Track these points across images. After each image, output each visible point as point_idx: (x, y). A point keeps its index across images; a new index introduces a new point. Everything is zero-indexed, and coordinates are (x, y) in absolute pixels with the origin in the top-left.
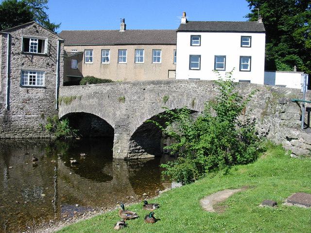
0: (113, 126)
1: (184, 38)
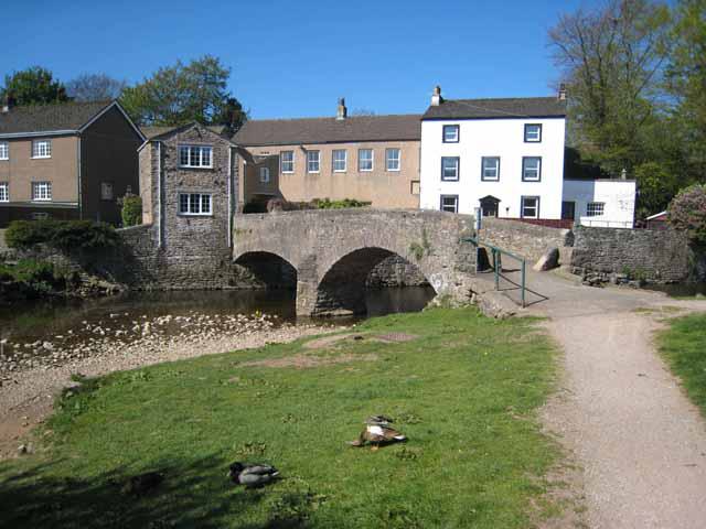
0: (296, 267)
1: (432, 130)
